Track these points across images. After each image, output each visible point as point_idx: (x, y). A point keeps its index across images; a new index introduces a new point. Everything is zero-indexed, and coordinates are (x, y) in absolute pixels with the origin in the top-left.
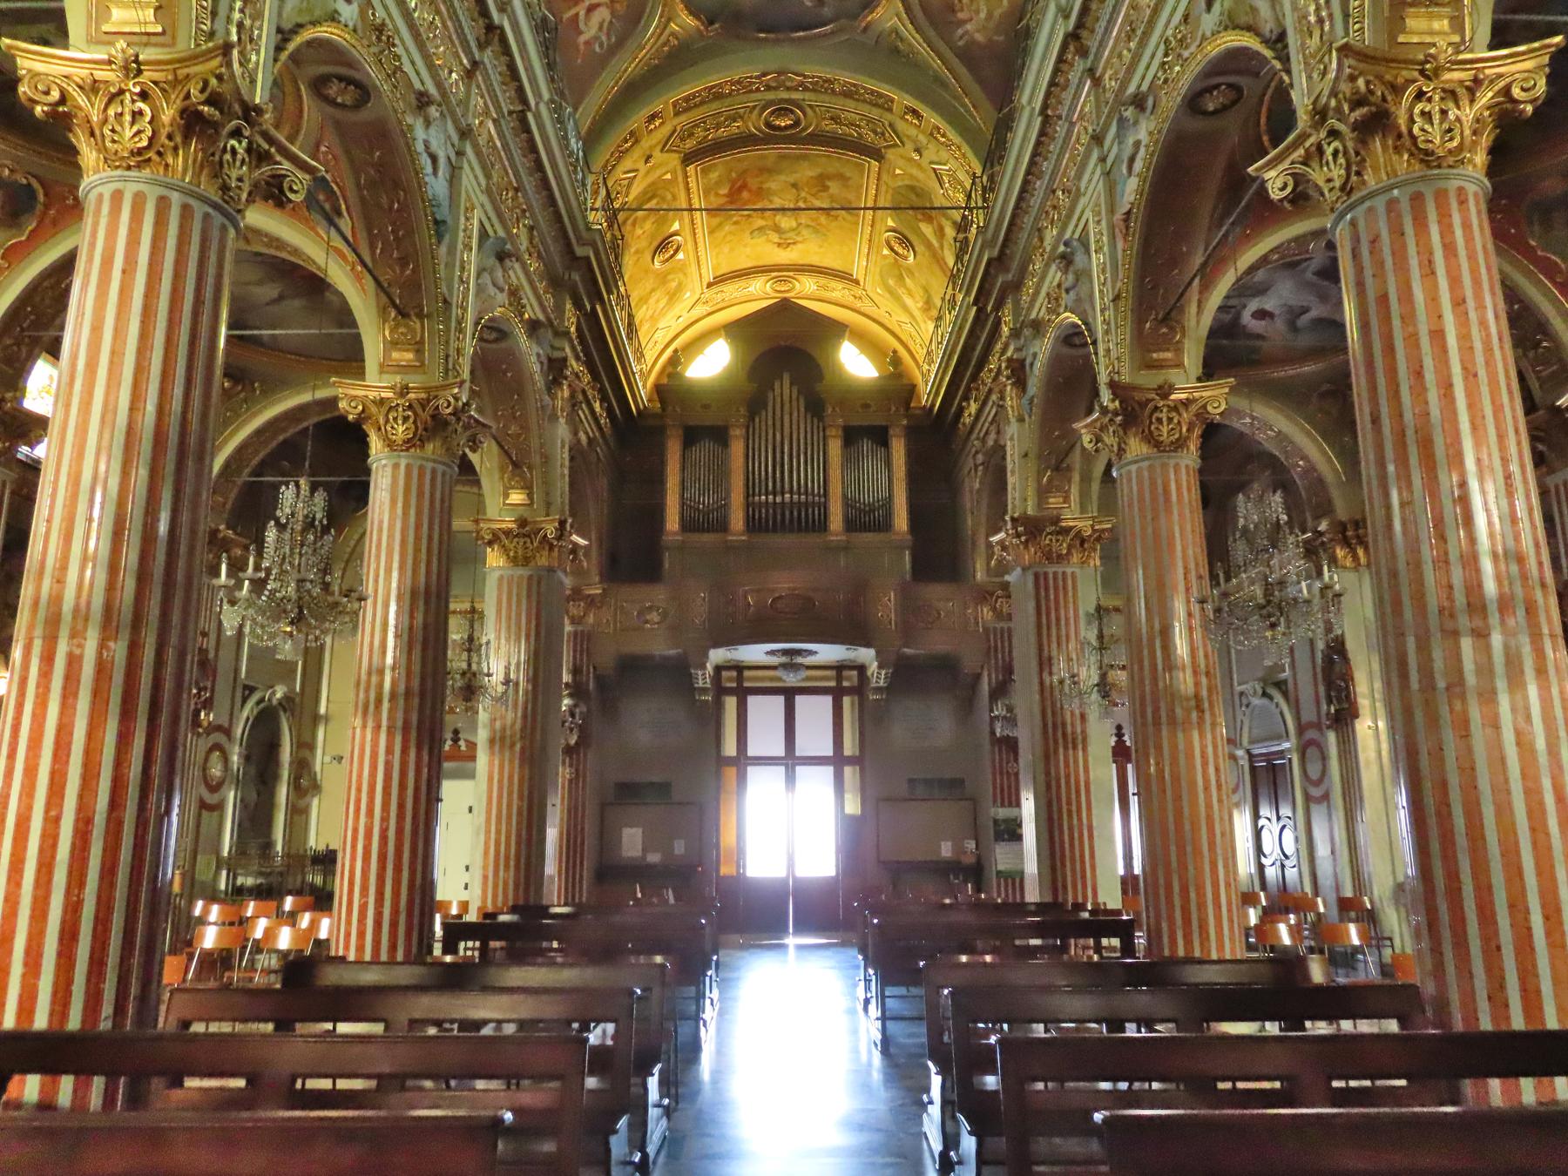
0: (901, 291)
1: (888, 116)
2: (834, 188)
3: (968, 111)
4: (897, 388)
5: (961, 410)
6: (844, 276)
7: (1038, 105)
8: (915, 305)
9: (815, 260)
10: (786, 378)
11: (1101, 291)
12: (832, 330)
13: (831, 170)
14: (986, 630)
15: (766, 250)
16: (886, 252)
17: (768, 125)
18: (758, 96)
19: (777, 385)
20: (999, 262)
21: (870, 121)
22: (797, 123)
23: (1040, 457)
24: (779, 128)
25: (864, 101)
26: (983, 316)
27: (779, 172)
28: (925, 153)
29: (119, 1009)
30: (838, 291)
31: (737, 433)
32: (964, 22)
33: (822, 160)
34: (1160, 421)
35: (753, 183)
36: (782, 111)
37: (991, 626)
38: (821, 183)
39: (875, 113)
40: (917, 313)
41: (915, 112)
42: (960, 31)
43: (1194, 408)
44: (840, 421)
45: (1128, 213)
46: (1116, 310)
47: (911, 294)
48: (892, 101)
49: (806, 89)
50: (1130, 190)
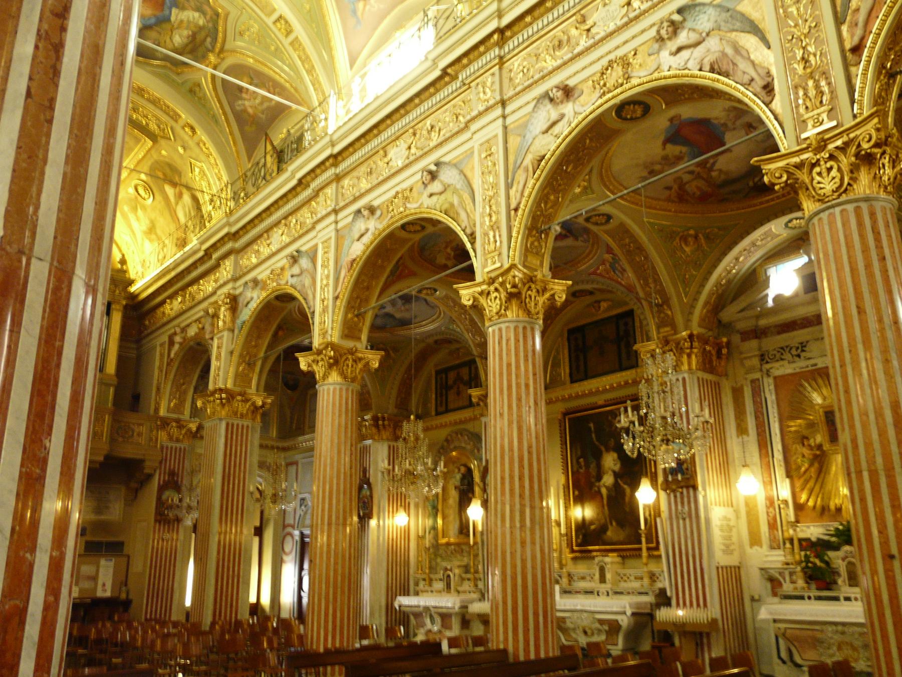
1: (174, 124)
5: (163, 302)
7: (299, 175)
14: (162, 447)
21: (158, 119)
23: (241, 356)
25: (162, 109)
26: (206, 258)
28: (188, 151)
29: (334, 638)
32: (245, 99)
34: (348, 366)
37: (165, 444)
39: (164, 118)
40: (139, 235)
41: (193, 129)
42: (240, 102)
43: (363, 362)
45: (354, 260)
47: (138, 219)
48: (180, 117)
50: (358, 249)
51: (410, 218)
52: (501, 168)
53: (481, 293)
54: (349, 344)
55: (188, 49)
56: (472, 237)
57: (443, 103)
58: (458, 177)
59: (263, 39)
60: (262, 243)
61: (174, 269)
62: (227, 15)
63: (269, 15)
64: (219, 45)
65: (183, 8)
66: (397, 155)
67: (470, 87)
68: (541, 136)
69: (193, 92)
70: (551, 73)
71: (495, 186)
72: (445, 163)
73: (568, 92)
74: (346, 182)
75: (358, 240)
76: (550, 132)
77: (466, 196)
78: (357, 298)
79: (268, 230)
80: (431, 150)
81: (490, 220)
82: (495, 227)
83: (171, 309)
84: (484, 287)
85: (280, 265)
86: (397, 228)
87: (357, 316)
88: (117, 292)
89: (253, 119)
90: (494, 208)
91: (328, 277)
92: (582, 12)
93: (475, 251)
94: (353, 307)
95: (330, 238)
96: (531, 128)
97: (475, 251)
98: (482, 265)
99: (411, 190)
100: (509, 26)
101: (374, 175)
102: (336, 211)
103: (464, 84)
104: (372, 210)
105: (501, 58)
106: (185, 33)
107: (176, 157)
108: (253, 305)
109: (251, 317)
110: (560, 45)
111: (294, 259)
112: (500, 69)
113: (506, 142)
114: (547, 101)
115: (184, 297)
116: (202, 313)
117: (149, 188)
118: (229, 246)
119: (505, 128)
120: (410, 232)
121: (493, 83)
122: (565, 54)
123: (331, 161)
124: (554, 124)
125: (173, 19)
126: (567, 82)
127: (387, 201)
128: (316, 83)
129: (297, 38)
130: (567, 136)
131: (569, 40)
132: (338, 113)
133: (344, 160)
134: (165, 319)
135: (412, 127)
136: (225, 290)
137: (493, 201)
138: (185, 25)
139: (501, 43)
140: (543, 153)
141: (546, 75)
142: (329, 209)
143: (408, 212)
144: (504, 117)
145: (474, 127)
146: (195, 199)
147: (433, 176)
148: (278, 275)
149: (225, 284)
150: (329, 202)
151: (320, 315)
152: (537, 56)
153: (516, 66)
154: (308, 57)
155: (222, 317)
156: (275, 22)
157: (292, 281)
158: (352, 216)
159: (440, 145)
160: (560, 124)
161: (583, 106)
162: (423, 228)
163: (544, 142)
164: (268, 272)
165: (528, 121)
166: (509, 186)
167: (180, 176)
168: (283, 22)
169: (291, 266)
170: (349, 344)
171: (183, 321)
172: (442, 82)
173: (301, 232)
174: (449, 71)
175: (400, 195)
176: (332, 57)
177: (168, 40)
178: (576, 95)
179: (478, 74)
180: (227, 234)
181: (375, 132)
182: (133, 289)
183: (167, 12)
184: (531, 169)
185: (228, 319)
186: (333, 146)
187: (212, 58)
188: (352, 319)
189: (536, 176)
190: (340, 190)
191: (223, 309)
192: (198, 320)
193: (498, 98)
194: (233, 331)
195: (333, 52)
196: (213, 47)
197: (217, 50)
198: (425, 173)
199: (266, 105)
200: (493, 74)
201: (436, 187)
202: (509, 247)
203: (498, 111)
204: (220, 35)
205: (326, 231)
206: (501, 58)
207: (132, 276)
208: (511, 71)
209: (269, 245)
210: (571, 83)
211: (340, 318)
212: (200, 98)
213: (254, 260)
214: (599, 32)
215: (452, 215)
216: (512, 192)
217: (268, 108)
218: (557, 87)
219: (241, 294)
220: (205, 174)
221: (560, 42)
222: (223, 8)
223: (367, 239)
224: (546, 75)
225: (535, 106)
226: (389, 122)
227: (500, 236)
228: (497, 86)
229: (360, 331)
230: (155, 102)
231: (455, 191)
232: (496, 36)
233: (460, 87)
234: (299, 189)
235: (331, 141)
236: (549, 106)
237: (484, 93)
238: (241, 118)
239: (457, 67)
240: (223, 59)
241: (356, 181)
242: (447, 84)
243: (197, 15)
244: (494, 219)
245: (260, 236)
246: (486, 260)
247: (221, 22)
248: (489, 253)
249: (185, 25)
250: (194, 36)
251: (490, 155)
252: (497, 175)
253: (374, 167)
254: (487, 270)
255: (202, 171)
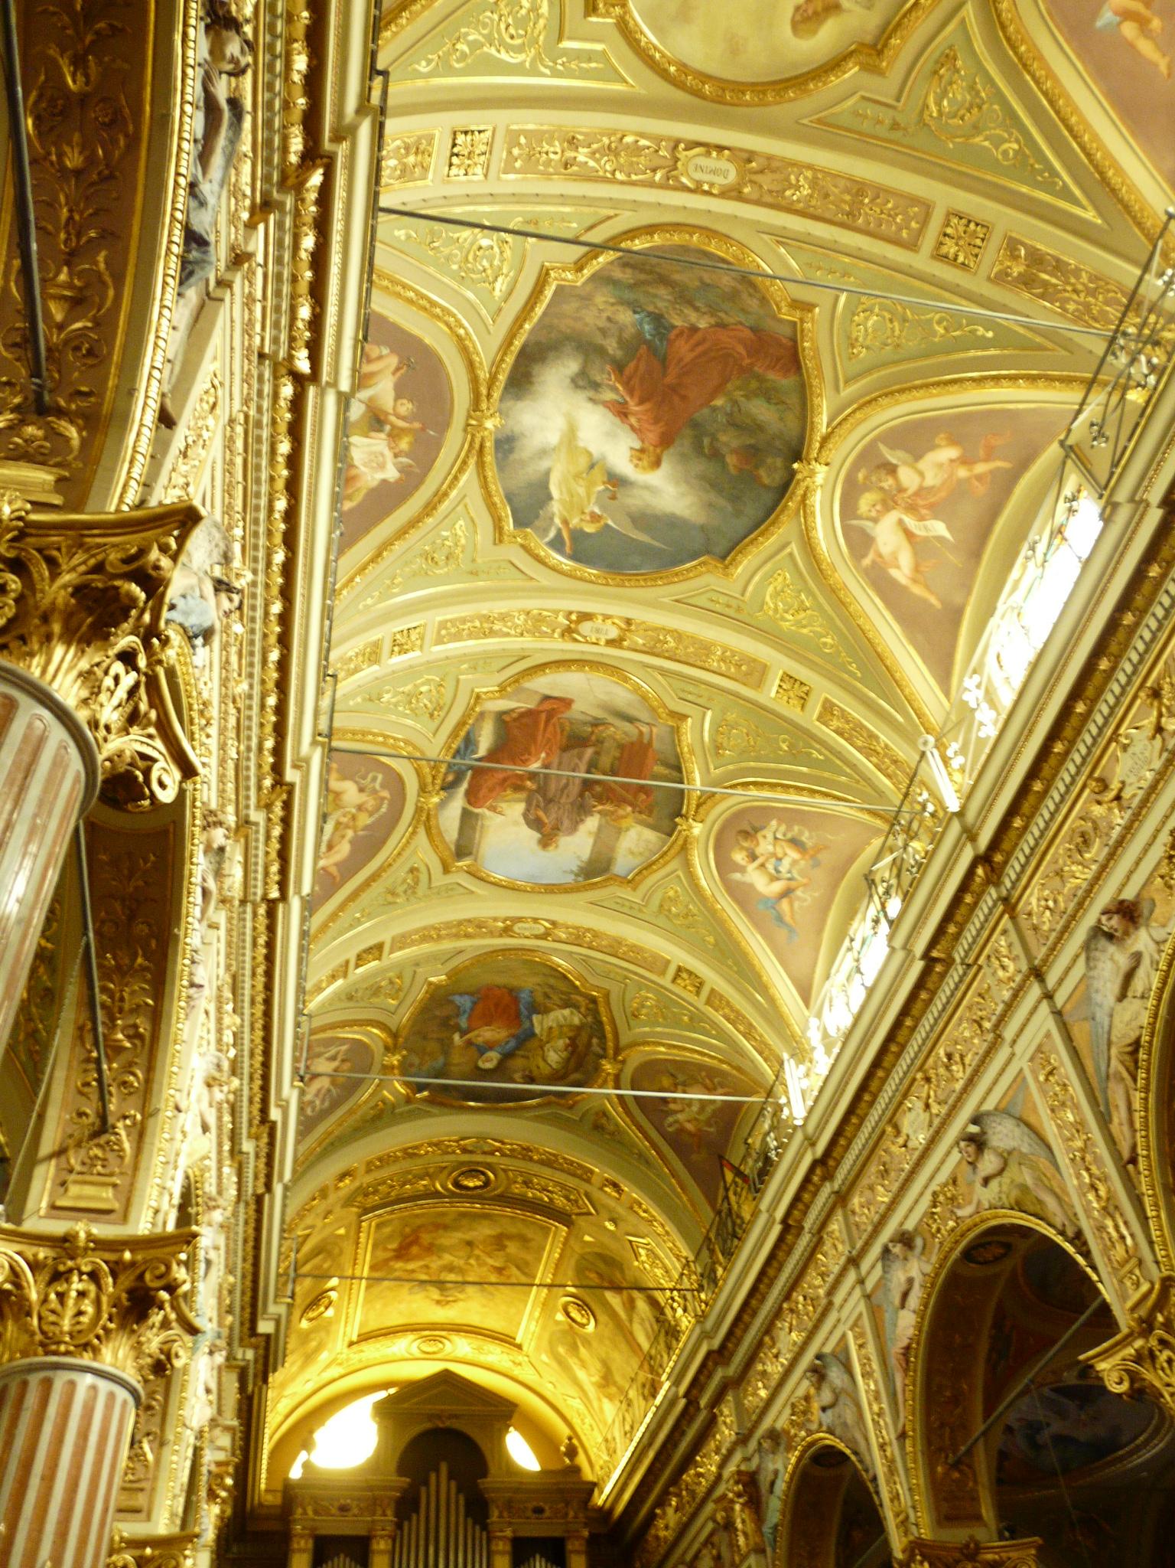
0: (573, 1362)
1: (585, 1186)
2: (512, 1248)
3: (673, 1190)
4: (567, 1484)
5: (652, 1517)
6: (506, 1339)
7: (779, 1214)
8: (588, 1378)
9: (475, 1319)
10: (444, 1468)
11: (876, 1423)
12: (500, 1412)
13: (512, 1230)
15: (423, 1307)
16: (560, 1317)
17: (457, 1184)
18: (452, 1158)
19: (433, 1477)
20: (719, 1355)
21: (563, 1187)
22: (487, 1183)
24: (467, 1188)
26: (692, 1409)
27: (456, 1229)
28: (621, 1224)
30: (496, 1355)
31: (381, 1545)
32: (676, 1112)
33: (508, 1218)
35: (426, 1238)
36: (473, 1172)
38: (499, 1242)
39: (572, 1182)
41: (615, 1186)
42: (670, 1119)
44: (508, 1533)
45: (908, 1348)
46: (902, 1448)
47: (583, 1364)
48: (592, 1172)
49: (503, 1155)
50: (906, 1324)
51: (971, 1235)
52: (1077, 1090)
53: (1138, 1359)
54: (958, 1535)
55: (572, 1064)
56: (1078, 1238)
57: (950, 1009)
58: (1017, 1132)
59: (667, 1010)
60: (766, 1354)
61: (650, 1444)
62: (607, 996)
63: (663, 973)
64: (610, 1044)
65: (546, 1011)
66: (915, 1126)
67: (980, 967)
68: (1119, 1007)
69: (598, 1127)
70: (1089, 892)
71: (1080, 1126)
72: (988, 1114)
73: (1129, 913)
74: (856, 1201)
75: (903, 1306)
76: (1130, 994)
77: (1043, 1163)
78: (942, 1425)
79: (769, 1329)
80: (959, 1099)
81: (1098, 1196)
82: (1111, 1209)
83: (667, 1527)
84: (1139, 1343)
85: (801, 1392)
86: (956, 1261)
87: (956, 1466)
88: (571, 1514)
89: (699, 1137)
90: (1094, 1169)
91: (877, 1394)
92: (1096, 775)
93: (1094, 1268)
94: (941, 1449)
95: (860, 1315)
96: (1098, 998)
97: (1094, 1268)
98: (1120, 1293)
99: (955, 1182)
100: (995, 844)
101: (893, 1174)
102: (854, 1261)
103: (969, 966)
104: (905, 1239)
105: (1005, 900)
106: (561, 1043)
107: (606, 1240)
108: (781, 1486)
109: (783, 1514)
110: (1086, 842)
111: (818, 1373)
112: (1013, 918)
113: (1068, 1038)
114: (1103, 942)
115: (678, 1495)
116: (710, 1526)
117: (584, 1306)
118: (719, 1374)
119: (1058, 1014)
120: (986, 1263)
121: (1010, 946)
122: (1097, 851)
123: (818, 1171)
124: (1129, 977)
125: (537, 1030)
126: (1123, 897)
127: (925, 1215)
128: (763, 1048)
129: (713, 991)
130: (1161, 990)
131: (1096, 828)
132: (803, 1089)
133: (838, 1163)
134: (662, 1551)
135: (920, 1069)
136: (731, 1468)
137: (1088, 1158)
138: (556, 1033)
139: (995, 875)
140: (1133, 1035)
141: (1084, 898)
142: (843, 1260)
143: (963, 1227)
144: (1049, 996)
145: (1009, 1033)
146: (654, 1303)
147: (978, 1143)
148: (804, 1413)
149: (731, 1452)
150: (840, 1247)
151: (888, 1483)
152: (1059, 873)
153: (1034, 901)
154: (738, 1014)
155: (739, 1526)
156: (674, 981)
157: (828, 1418)
158: (879, 1265)
159: (970, 1083)
160: (1141, 973)
161: (1164, 926)
162: (1008, 1247)
163: (1127, 1017)
164: (788, 1411)
165: (1088, 987)
166: (1104, 1120)
167: (622, 1271)
168: (684, 975)
169: (818, 1389)
170: (958, 1535)
171: (685, 1553)
172: (934, 977)
173: (817, 1316)
174: (935, 954)
175: (941, 1198)
176: (771, 1000)
177: (542, 1064)
178: (1146, 912)
179: (981, 941)
180: (709, 1354)
181: (867, 1097)
182: (600, 1499)
183: (527, 1025)
184: (1125, 1075)
185: (750, 1527)
186: (813, 1144)
187: (608, 1067)
188: (946, 1474)
189: (1140, 1083)
190: (852, 1219)
191: (737, 1507)
192: (708, 1542)
193: (1024, 967)
194: (763, 1551)
195: (772, 991)
196: (604, 1049)
197: (611, 1052)
198: (963, 1144)
199: (709, 1109)
200: (1005, 932)
201: (989, 1163)
202: (1151, 1243)
203: (1035, 991)
204: (608, 1028)
205: (850, 1305)
206: (1005, 900)
207: (588, 1475)
208: (1030, 914)
209: (776, 1356)
210: (1129, 894)
211: (920, 1480)
212: (612, 1134)
213: (763, 1393)
214: (1133, 793)
215: (1031, 1209)
216: (1115, 1127)
217: (714, 1113)
218: (1106, 912)
219: (759, 1467)
220: (657, 1257)
221: (1083, 835)
222: (598, 988)
223: (914, 1301)
224: (1084, 898)
225: (1088, 959)
226: (880, 1073)
227: (1126, 1223)
228: (1018, 950)
229: (975, 1499)
230: (549, 1162)
231: (1023, 1160)
232: (980, 871)
233: (965, 974)
234: (789, 1238)
235: (807, 1138)
236: (1112, 949)
237: (1004, 968)
238: (680, 1143)
239: (944, 943)
240: (623, 1062)
241: (868, 1193)
242: (943, 976)
243: (567, 1012)
244: (1102, 1192)
245: (759, 1345)
246: (1121, 1282)
247: (602, 1009)
248: (1122, 1265)
249: (556, 1033)
250: (573, 1043)
251: (1051, 1073)
252: (1076, 1107)
253: (887, 1158)
254: (1130, 1304)
255: (651, 1252)
